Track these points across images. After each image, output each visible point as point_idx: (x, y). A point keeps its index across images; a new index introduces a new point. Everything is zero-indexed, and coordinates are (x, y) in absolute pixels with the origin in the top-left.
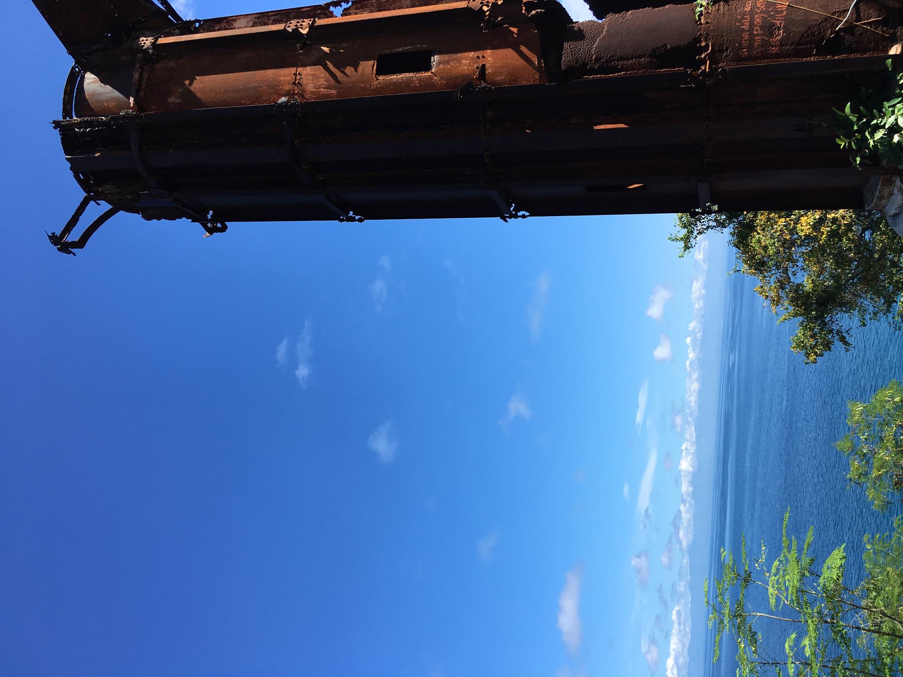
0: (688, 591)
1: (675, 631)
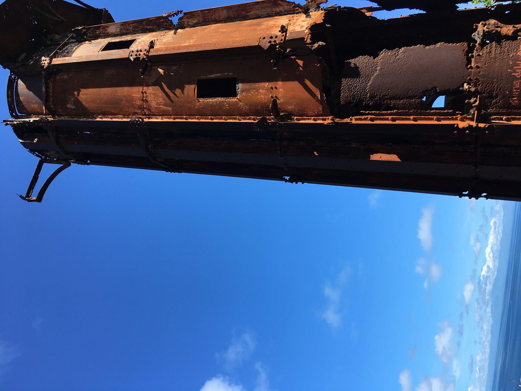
0: (502, 209)
1: (492, 232)
